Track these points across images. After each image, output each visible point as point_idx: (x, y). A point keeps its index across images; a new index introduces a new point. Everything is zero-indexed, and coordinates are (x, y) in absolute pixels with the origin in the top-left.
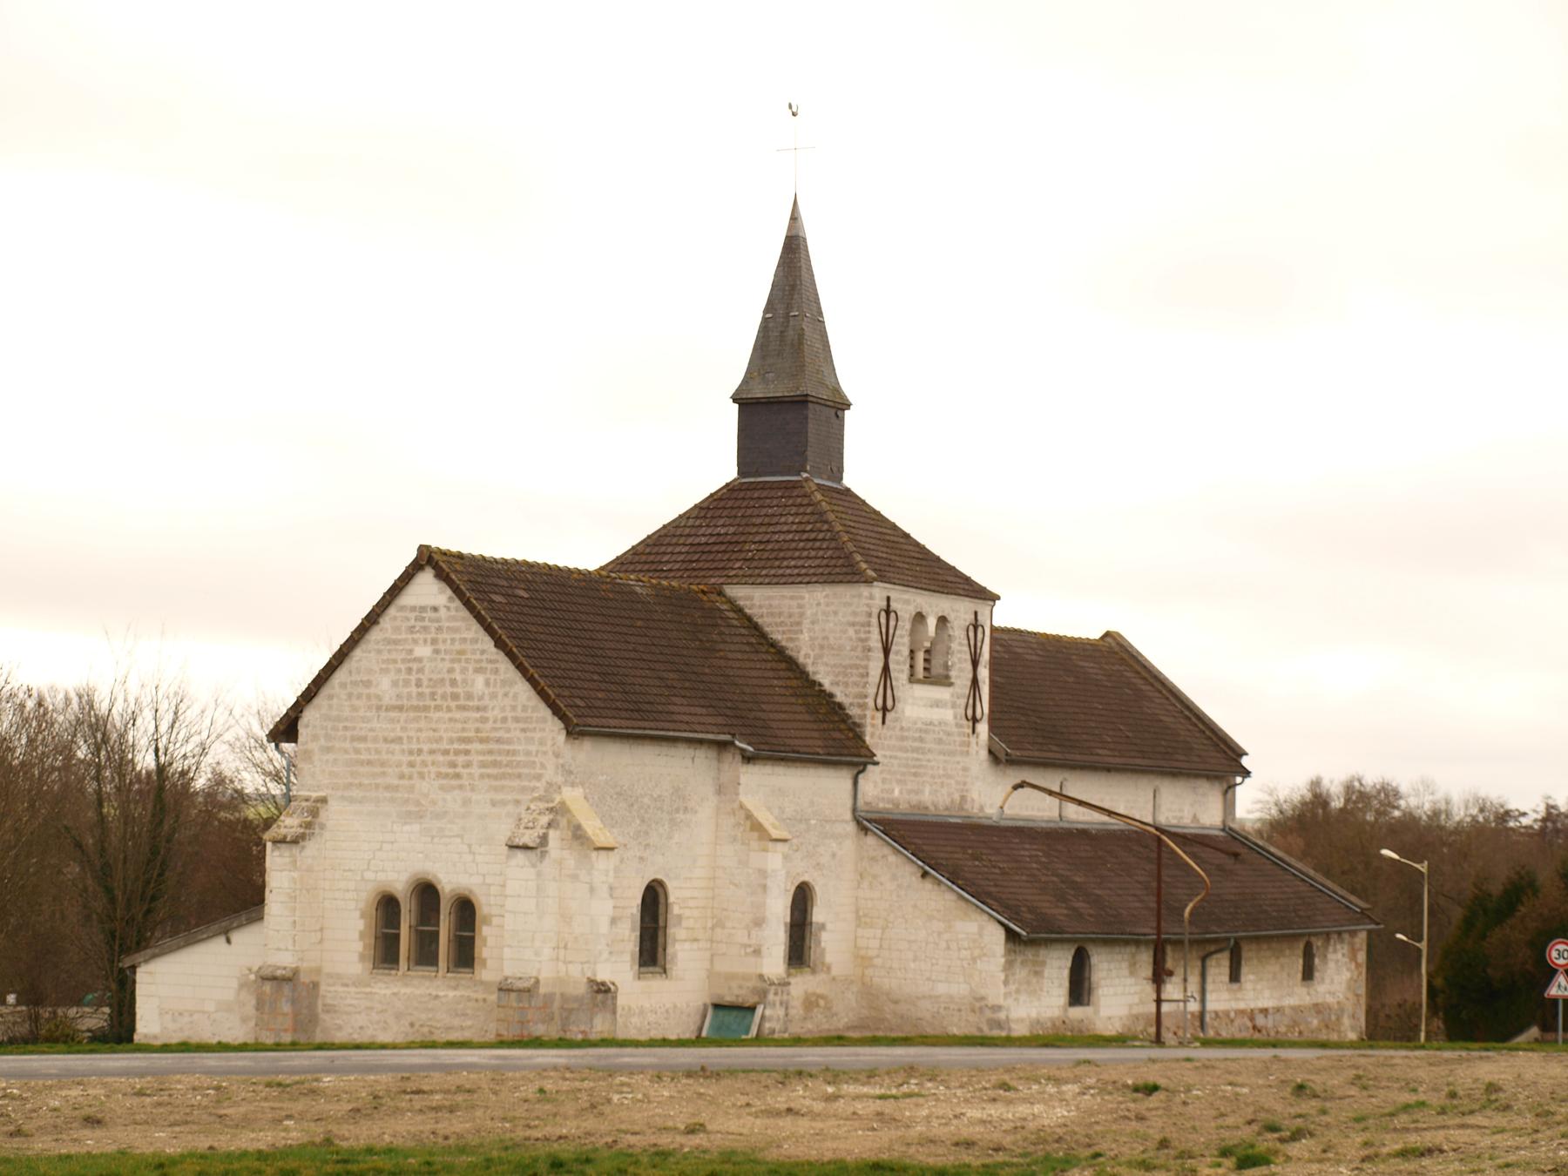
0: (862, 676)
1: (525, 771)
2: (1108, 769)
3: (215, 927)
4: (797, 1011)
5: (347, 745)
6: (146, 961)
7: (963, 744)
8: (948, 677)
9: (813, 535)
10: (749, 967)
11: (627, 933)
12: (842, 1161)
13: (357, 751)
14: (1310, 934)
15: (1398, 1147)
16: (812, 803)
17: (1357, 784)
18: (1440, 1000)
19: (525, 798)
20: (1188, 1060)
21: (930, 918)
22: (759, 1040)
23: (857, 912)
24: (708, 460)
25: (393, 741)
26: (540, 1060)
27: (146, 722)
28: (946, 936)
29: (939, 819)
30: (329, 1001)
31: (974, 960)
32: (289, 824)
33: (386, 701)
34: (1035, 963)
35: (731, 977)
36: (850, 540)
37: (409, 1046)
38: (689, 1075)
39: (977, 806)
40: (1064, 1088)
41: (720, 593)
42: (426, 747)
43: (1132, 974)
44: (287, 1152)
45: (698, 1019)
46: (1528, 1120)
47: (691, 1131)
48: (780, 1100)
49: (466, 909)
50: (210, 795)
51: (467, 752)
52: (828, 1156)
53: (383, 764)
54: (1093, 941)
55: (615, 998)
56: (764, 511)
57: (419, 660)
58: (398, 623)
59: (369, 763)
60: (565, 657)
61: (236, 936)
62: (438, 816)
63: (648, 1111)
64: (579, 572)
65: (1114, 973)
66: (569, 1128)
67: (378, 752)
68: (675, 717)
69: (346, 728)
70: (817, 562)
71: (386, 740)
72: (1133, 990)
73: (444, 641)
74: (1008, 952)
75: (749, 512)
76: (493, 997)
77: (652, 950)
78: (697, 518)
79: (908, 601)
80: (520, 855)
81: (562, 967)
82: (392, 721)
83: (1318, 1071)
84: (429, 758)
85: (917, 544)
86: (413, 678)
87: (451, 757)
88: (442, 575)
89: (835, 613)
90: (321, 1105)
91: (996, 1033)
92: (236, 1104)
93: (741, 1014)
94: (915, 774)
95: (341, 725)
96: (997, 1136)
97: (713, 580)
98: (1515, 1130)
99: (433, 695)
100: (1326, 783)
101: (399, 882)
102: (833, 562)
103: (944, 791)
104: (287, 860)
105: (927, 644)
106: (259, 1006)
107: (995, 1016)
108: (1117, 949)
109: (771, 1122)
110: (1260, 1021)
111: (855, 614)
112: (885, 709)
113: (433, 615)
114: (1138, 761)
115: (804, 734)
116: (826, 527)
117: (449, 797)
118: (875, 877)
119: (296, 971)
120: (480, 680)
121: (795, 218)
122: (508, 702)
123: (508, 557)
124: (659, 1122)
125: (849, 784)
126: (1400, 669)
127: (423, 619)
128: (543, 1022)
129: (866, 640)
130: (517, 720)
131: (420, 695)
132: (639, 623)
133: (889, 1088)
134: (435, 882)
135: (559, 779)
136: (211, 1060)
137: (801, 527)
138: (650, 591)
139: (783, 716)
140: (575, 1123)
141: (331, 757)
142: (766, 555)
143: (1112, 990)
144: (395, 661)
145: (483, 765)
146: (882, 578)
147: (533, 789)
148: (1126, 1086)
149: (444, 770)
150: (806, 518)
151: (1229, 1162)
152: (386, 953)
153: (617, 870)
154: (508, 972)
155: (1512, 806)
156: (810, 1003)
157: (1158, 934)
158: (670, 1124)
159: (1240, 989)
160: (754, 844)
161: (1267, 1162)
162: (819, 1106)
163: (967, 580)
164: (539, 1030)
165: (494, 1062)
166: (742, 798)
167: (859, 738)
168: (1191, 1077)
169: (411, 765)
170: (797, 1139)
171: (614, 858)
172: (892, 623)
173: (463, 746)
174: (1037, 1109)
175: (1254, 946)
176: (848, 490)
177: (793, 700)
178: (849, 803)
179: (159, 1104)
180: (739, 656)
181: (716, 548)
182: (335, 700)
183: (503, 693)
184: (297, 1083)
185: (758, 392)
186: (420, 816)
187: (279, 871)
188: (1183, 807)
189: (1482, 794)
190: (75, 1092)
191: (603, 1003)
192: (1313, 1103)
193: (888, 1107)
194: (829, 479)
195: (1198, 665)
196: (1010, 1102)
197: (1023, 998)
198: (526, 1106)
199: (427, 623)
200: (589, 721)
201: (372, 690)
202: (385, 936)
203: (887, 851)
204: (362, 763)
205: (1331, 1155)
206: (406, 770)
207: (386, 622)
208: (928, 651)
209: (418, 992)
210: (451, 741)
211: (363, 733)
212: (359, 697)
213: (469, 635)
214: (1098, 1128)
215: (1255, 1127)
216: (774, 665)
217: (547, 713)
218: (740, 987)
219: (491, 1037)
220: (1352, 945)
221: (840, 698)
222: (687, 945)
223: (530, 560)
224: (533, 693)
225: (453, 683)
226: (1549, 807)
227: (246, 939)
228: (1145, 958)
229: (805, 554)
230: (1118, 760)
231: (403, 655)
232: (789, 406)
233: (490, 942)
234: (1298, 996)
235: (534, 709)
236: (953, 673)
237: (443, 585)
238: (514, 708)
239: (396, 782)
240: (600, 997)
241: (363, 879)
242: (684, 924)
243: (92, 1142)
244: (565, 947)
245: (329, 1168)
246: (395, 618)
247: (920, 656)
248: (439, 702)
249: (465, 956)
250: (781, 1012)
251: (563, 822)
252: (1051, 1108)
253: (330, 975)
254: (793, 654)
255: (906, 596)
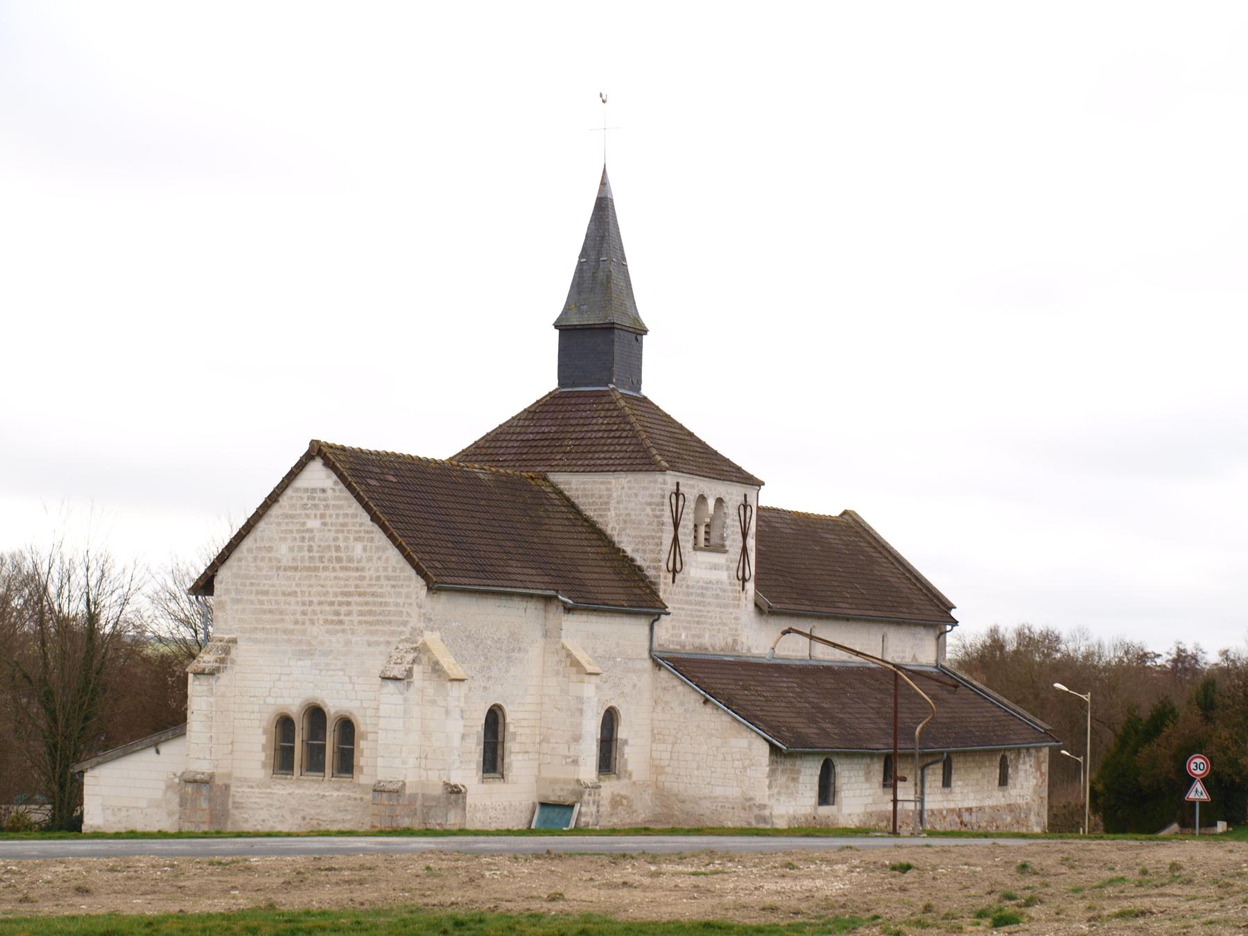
0: (657, 545)
1: (395, 618)
2: (847, 619)
3: (147, 741)
4: (606, 808)
5: (253, 597)
6: (92, 768)
7: (734, 599)
8: (723, 546)
9: (618, 434)
10: (568, 773)
11: (474, 746)
12: (677, 921)
13: (261, 602)
14: (1005, 750)
15: (1116, 910)
16: (618, 645)
17: (1027, 631)
18: (1100, 801)
19: (394, 639)
20: (928, 846)
21: (710, 735)
22: (579, 831)
23: (652, 730)
24: (536, 375)
25: (289, 595)
26: (414, 845)
27: (79, 577)
28: (723, 750)
29: (716, 658)
30: (238, 800)
31: (745, 768)
32: (207, 659)
33: (284, 563)
34: (792, 771)
35: (554, 781)
36: (648, 437)
37: (310, 834)
38: (538, 857)
39: (745, 648)
40: (836, 867)
41: (545, 479)
42: (315, 600)
43: (867, 780)
44: (242, 914)
45: (528, 814)
46: (1212, 890)
47: (552, 899)
48: (617, 876)
49: (347, 727)
50: (116, 636)
51: (348, 604)
52: (666, 918)
53: (281, 613)
54: (838, 754)
55: (465, 798)
56: (579, 414)
57: (311, 531)
58: (294, 502)
59: (271, 611)
60: (426, 528)
61: (164, 748)
62: (325, 654)
63: (516, 884)
64: (435, 461)
65: (853, 780)
66: (455, 896)
67: (277, 603)
68: (511, 577)
69: (252, 584)
70: (622, 455)
71: (284, 594)
72: (868, 792)
73: (331, 516)
74: (772, 762)
75: (568, 415)
76: (369, 797)
77: (492, 760)
78: (526, 419)
79: (693, 486)
80: (390, 684)
81: (423, 773)
82: (289, 578)
83: (1033, 855)
84: (318, 608)
85: (699, 441)
86: (306, 544)
87: (336, 608)
88: (328, 464)
89: (636, 495)
90: (256, 879)
91: (761, 826)
92: (188, 878)
93: (563, 811)
94: (698, 622)
95: (248, 582)
96: (793, 903)
97: (539, 469)
98: (1204, 897)
99: (321, 558)
100: (1002, 630)
101: (294, 705)
102: (634, 455)
103: (720, 636)
104: (205, 688)
105: (708, 520)
106: (182, 803)
107: (762, 813)
108: (856, 761)
109: (611, 892)
110: (966, 817)
111: (651, 496)
112: (675, 571)
113: (322, 495)
114: (871, 613)
115: (611, 590)
116: (628, 427)
117: (333, 639)
118: (666, 703)
119: (212, 776)
120: (359, 547)
121: (604, 183)
122: (381, 564)
123: (380, 450)
124: (526, 892)
125: (646, 629)
126: (1081, 537)
127: (314, 498)
128: (408, 816)
129: (661, 516)
130: (388, 578)
131: (311, 558)
132: (483, 502)
133: (699, 867)
134: (322, 705)
135: (422, 625)
136: (157, 845)
137: (609, 427)
138: (491, 477)
139: (596, 576)
140: (460, 893)
141: (240, 607)
142: (581, 449)
143: (851, 793)
144: (291, 532)
145: (361, 614)
146: (673, 468)
147: (401, 633)
148: (884, 866)
149: (330, 618)
150: (613, 420)
151: (987, 922)
152: (283, 761)
153: (466, 697)
154: (380, 777)
155: (1148, 650)
156: (616, 802)
157: (895, 748)
158: (535, 894)
159: (951, 792)
160: (574, 677)
161: (1018, 922)
162: (647, 881)
163: (739, 469)
164: (406, 822)
165: (378, 847)
166: (564, 640)
167: (655, 593)
168: (934, 860)
169: (304, 613)
170: (639, 904)
171: (464, 686)
172: (681, 503)
173: (345, 599)
174: (819, 883)
175: (961, 759)
176: (645, 398)
177: (603, 563)
178: (647, 645)
179: (130, 878)
180: (561, 528)
181: (541, 443)
182: (244, 563)
183: (377, 557)
184: (233, 862)
185: (575, 321)
186: (310, 654)
187: (200, 698)
188: (908, 649)
189: (1128, 641)
190: (60, 869)
191: (456, 802)
192: (1035, 878)
193: (701, 881)
194: (630, 389)
195: (914, 535)
196: (795, 878)
197: (783, 798)
198: (418, 880)
199: (317, 502)
200: (445, 579)
201: (273, 554)
202: (283, 748)
203: (676, 682)
204: (264, 612)
205: (1062, 916)
206: (300, 618)
207: (284, 500)
208: (708, 526)
209: (308, 792)
210: (336, 595)
211: (266, 588)
212: (263, 559)
213: (351, 511)
214: (870, 897)
215: (996, 896)
216: (588, 536)
217: (411, 572)
218: (562, 790)
219: (367, 827)
220: (1038, 758)
221: (639, 562)
222: (520, 757)
223: (397, 452)
224: (401, 557)
225: (338, 548)
226: (1180, 651)
227: (171, 750)
228: (878, 767)
229: (612, 448)
230: (856, 612)
231: (298, 527)
232: (599, 333)
233: (366, 753)
234: (996, 798)
235: (402, 570)
236: (727, 543)
237: (330, 472)
238: (385, 569)
239: (292, 627)
240: (453, 796)
241: (265, 703)
242: (518, 739)
243: (84, 906)
244: (426, 758)
245: (282, 926)
246: (292, 498)
247: (702, 529)
248: (326, 564)
249: (346, 764)
250: (594, 809)
251: (425, 659)
252: (830, 881)
253: (238, 779)
254: (602, 527)
255: (691, 482)
